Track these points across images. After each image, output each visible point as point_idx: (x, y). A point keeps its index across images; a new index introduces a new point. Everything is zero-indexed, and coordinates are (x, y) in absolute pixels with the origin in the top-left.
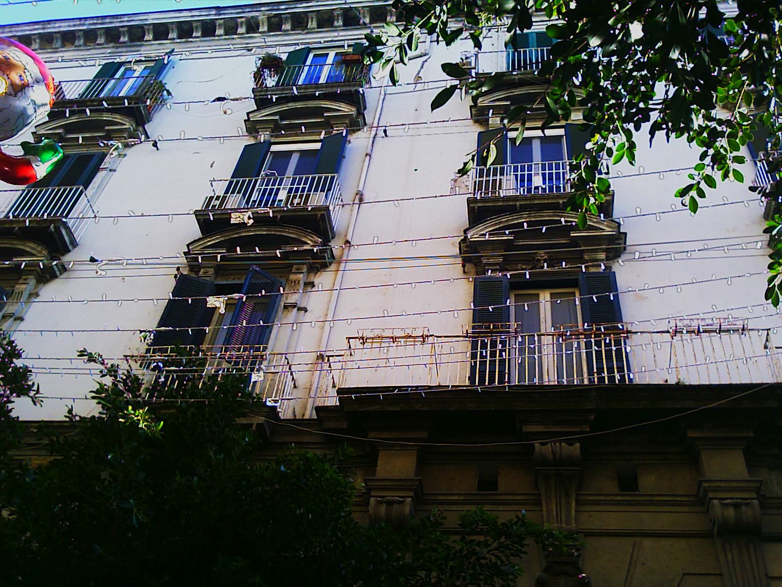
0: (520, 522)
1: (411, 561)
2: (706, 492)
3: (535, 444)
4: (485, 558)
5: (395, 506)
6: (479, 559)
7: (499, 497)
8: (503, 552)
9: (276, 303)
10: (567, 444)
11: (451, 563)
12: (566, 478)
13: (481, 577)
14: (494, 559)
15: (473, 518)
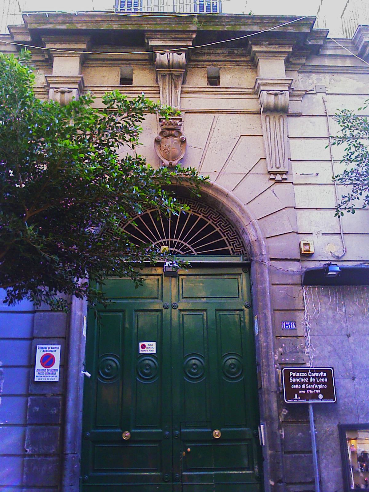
0: (141, 100)
1: (73, 125)
2: (259, 86)
3: (157, 54)
4: (120, 123)
5: (66, 94)
6: (115, 124)
7: (133, 89)
8: (130, 119)
9: (257, 375)
10: (178, 54)
11: (98, 126)
12: (176, 75)
13: (117, 134)
14: (125, 124)
15: (112, 98)
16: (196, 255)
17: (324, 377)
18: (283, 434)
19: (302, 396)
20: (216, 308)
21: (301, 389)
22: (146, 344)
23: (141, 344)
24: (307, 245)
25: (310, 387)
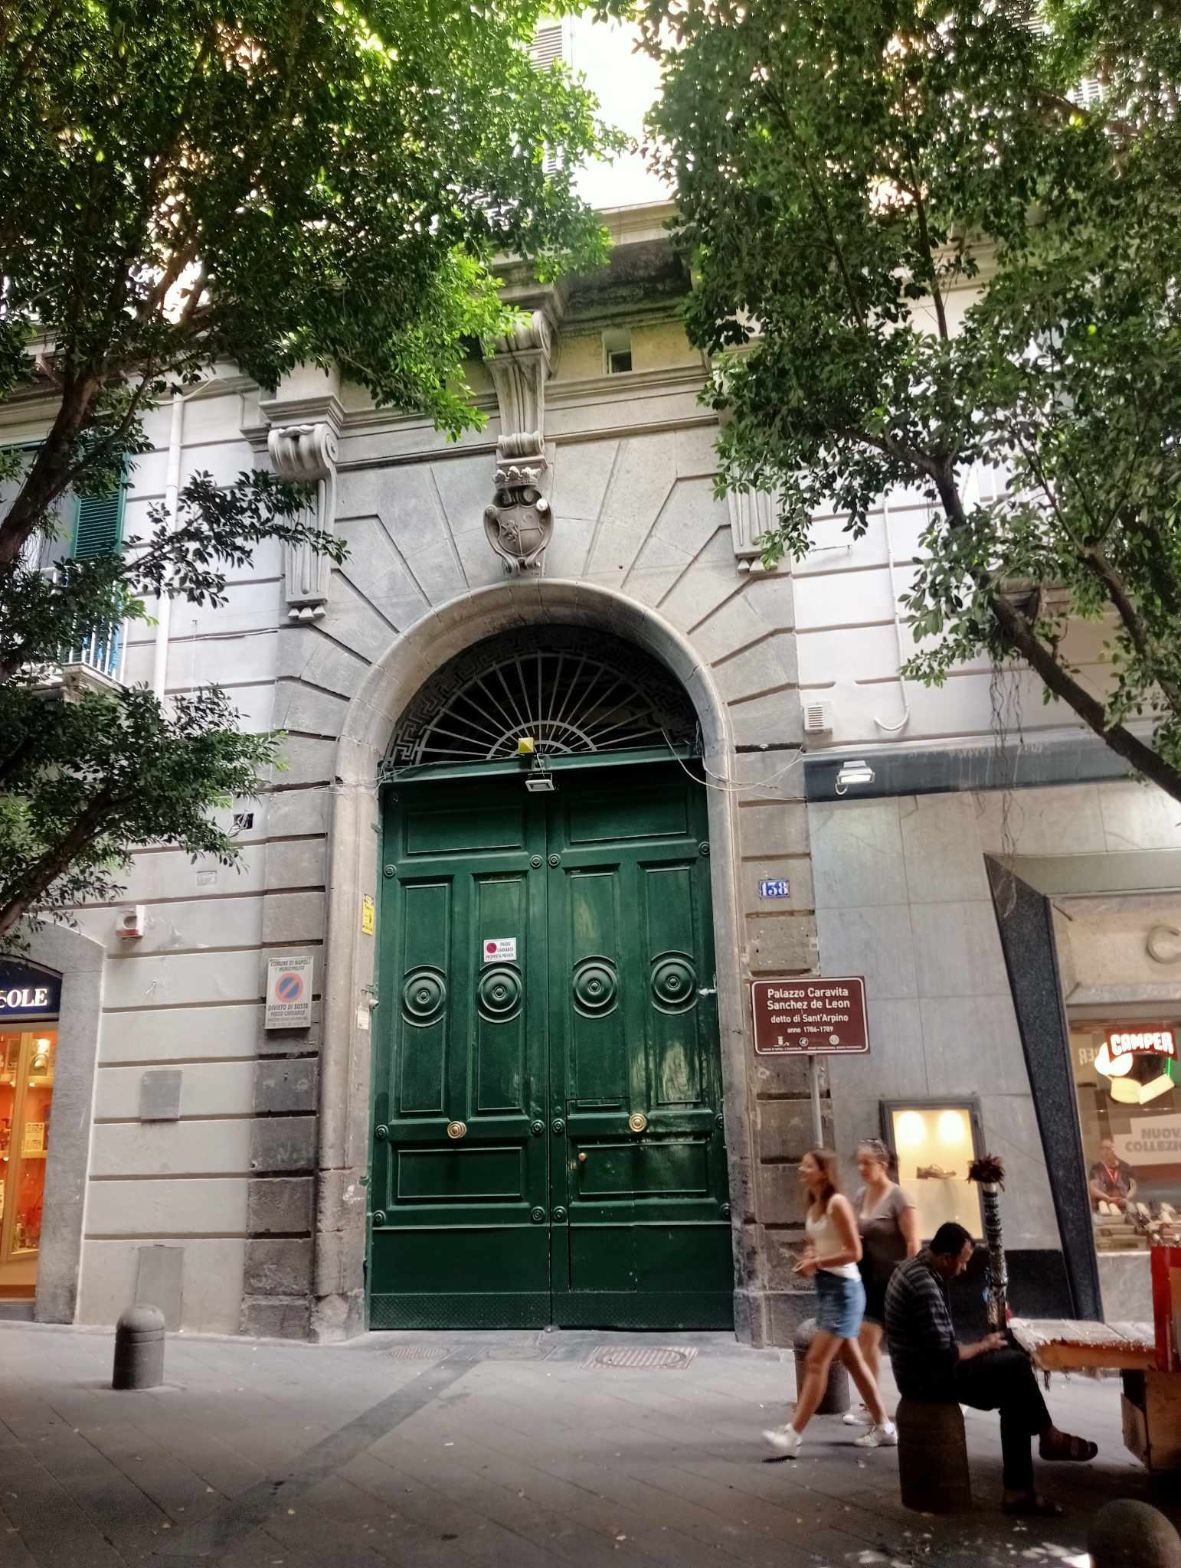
16: (594, 750)
17: (843, 998)
18: (759, 1121)
19: (793, 1040)
20: (641, 860)
21: (793, 1025)
22: (498, 942)
23: (486, 943)
24: (816, 712)
25: (811, 1019)
